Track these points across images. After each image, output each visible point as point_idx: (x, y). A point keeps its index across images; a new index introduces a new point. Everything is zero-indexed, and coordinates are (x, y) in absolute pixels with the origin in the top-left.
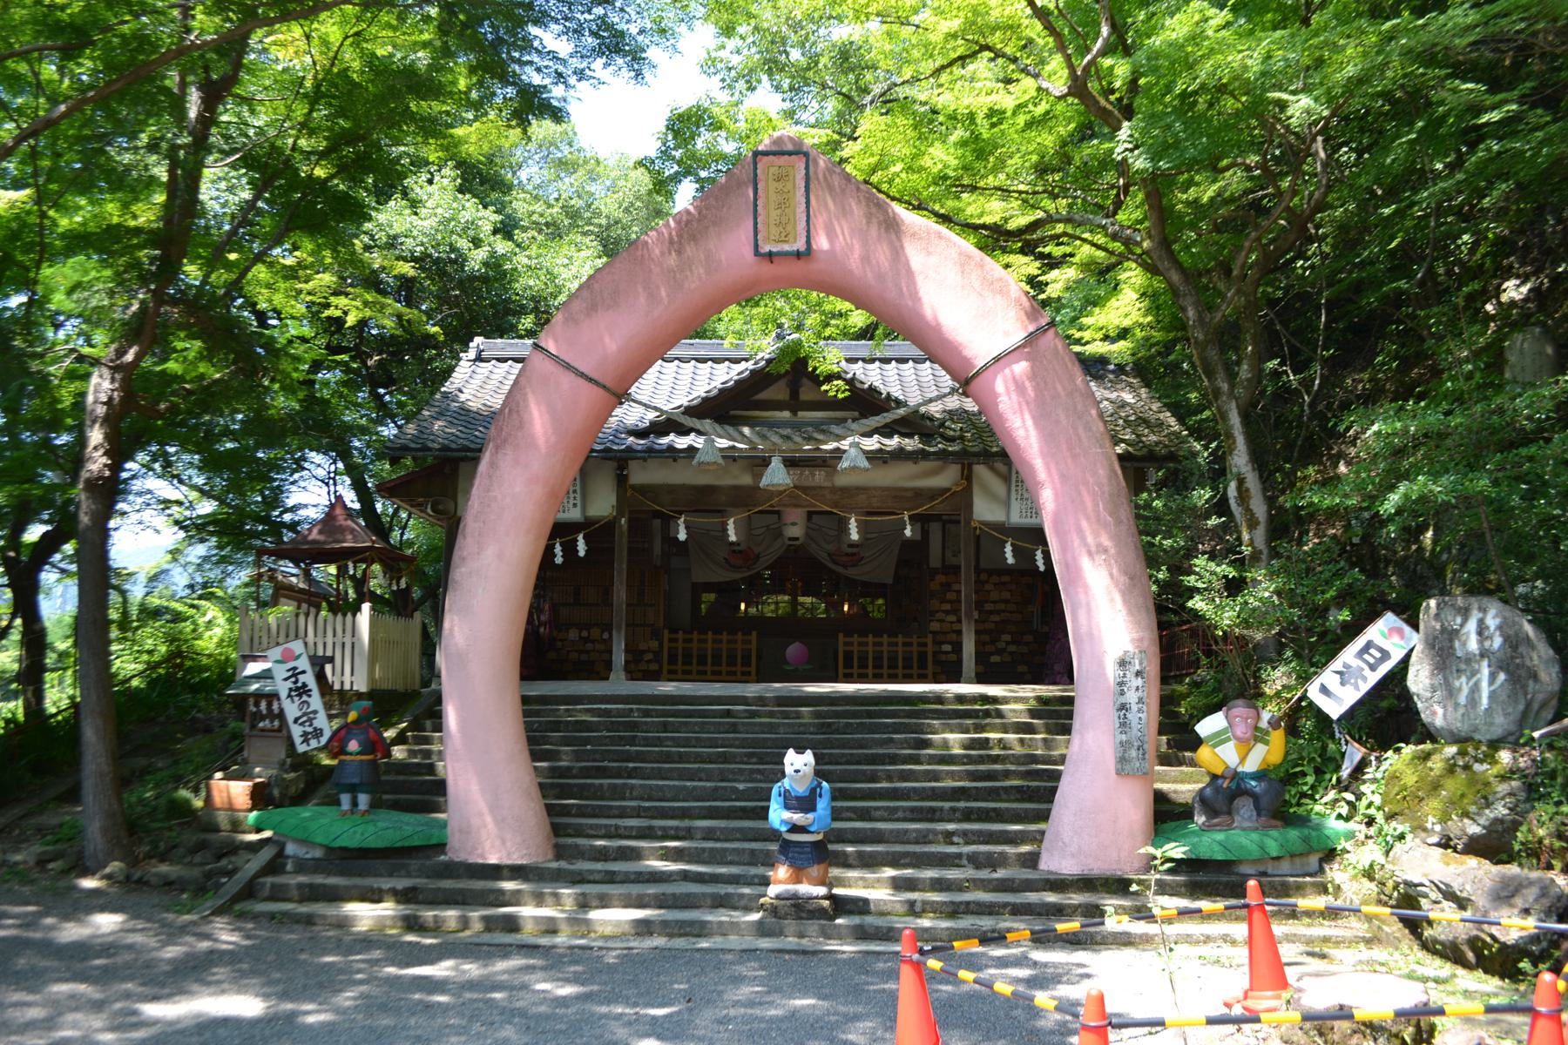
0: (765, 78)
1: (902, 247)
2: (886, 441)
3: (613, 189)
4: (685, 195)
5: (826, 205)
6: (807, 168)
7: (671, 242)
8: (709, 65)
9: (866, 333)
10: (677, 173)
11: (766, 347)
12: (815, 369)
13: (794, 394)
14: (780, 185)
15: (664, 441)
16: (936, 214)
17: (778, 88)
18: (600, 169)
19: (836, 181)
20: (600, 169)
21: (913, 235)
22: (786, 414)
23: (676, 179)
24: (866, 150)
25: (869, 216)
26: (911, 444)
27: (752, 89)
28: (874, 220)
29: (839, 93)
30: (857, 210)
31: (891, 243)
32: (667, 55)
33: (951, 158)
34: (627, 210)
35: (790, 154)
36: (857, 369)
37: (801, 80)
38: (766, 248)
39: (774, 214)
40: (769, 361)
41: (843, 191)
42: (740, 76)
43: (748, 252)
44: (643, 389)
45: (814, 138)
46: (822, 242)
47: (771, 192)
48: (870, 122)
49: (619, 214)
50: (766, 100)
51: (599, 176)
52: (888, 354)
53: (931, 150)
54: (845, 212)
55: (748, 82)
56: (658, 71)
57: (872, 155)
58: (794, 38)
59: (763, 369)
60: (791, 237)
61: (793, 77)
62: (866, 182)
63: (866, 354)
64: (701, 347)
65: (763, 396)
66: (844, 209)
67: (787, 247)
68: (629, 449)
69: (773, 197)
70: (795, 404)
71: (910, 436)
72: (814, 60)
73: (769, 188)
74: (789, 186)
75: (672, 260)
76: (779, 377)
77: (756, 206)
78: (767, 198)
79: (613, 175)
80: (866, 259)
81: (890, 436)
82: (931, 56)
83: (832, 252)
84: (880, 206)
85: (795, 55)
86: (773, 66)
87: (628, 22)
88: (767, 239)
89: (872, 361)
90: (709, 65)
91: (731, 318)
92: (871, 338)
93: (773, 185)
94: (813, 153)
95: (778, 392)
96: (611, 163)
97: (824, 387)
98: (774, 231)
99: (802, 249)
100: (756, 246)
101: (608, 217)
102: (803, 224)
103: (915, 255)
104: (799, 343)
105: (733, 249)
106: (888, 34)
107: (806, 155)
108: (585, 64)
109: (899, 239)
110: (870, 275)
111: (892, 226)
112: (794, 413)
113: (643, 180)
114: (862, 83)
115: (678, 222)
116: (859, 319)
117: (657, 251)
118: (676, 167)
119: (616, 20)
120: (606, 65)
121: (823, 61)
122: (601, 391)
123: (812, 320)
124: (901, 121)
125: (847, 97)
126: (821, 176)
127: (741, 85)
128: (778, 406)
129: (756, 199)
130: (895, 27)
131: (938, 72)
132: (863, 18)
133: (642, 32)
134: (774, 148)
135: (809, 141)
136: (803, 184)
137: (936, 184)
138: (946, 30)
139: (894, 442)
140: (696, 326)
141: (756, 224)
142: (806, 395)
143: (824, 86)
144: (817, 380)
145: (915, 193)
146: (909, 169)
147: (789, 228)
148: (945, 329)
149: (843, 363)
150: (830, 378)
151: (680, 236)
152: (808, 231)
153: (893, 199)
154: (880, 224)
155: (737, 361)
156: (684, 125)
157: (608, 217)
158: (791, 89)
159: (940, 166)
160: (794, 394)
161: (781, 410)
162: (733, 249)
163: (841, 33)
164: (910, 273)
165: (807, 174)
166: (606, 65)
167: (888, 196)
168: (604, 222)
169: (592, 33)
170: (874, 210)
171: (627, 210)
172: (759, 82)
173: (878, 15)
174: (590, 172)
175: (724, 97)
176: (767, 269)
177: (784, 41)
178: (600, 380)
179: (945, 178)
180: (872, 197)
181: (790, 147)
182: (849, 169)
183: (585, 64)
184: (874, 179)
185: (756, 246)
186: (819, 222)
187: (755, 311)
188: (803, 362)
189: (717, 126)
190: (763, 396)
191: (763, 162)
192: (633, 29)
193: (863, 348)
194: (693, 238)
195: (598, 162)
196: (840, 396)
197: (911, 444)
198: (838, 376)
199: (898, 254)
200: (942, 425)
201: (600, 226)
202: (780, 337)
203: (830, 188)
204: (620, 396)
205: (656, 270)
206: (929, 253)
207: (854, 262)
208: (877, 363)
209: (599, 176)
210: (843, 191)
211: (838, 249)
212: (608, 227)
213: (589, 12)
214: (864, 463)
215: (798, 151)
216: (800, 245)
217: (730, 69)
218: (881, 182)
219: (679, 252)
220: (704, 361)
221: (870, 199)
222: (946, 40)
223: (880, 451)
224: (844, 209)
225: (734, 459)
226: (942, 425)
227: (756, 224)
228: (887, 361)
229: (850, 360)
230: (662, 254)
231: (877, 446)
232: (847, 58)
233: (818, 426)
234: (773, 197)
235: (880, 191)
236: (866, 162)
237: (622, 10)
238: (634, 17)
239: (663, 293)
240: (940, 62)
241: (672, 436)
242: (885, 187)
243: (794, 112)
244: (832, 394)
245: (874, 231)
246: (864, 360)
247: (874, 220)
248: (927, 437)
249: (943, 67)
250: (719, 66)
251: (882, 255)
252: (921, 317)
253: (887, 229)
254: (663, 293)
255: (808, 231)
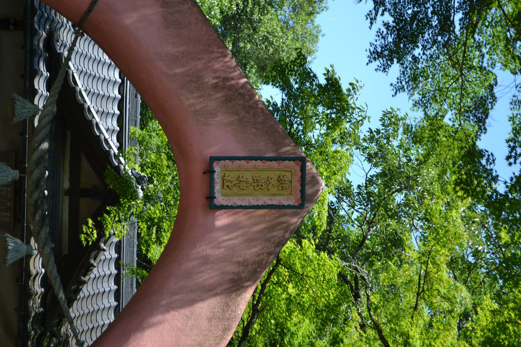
0: (379, 170)
1: (216, 295)
2: (38, 281)
3: (286, 27)
4: (270, 94)
5: (256, 224)
6: (289, 207)
7: (226, 79)
8: (390, 119)
9: (144, 261)
10: (291, 87)
11: (130, 167)
12: (109, 213)
13: (86, 193)
14: (274, 182)
15: (42, 67)
16: (250, 323)
17: (370, 181)
18: (303, 16)
19: (278, 233)
20: (303, 16)
21: (227, 305)
22: (66, 185)
23: (286, 87)
24: (308, 260)
25: (244, 264)
26: (35, 305)
27: (370, 158)
28: (241, 269)
29: (365, 238)
30: (251, 253)
31: (220, 284)
32: (394, 81)
33: (300, 339)
34: (265, 38)
35: (303, 191)
36: (109, 253)
37: (374, 200)
38: (217, 168)
39: (248, 176)
40: (117, 169)
41: (268, 240)
42: (381, 147)
43: (214, 151)
44: (86, 46)
45: (319, 214)
46: (222, 220)
47: (270, 174)
48: (332, 265)
49: (262, 31)
50: (358, 171)
51: (297, 15)
52: (124, 281)
53: (307, 321)
54: (250, 241)
55: (376, 154)
56: (380, 73)
57: (303, 267)
58: (412, 196)
59: (111, 163)
60: (227, 191)
61: (379, 195)
62: (279, 261)
63: (124, 261)
64: (134, 103)
65: (85, 164)
66: (252, 240)
67: (218, 187)
68: (34, 33)
69: (264, 175)
70: (76, 193)
71: (43, 304)
72: (395, 215)
73: (271, 171)
74: (274, 190)
75: (210, 80)
76: (102, 178)
77: (256, 159)
78: (263, 170)
79: (299, 28)
80: (206, 260)
81: (42, 285)
82: (390, 321)
83: (213, 229)
84: (253, 276)
85: (399, 198)
86: (390, 177)
87: (424, 48)
88: (225, 169)
89: (118, 267)
90: (390, 119)
91: (157, 136)
92: (139, 265)
93: (274, 175)
94: (303, 212)
95: (88, 177)
96: (309, 26)
97: (90, 222)
98: (232, 176)
99: (216, 202)
100: (219, 159)
101: (260, 21)
102: (239, 203)
103: (205, 308)
104: (135, 197)
105: (217, 137)
106: (410, 281)
107: (301, 206)
108: (389, 6)
109: (222, 293)
110: (191, 264)
111: (236, 285)
112: (68, 192)
113: (287, 55)
114: (373, 258)
115: (244, 86)
116: (155, 252)
117: (217, 66)
118: (296, 86)
119: (426, 36)
120: (386, 25)
121: (393, 223)
122: (85, 7)
123: (155, 211)
124: (333, 294)
125: (361, 244)
126: (282, 219)
127: (374, 148)
128: (75, 178)
129: (262, 159)
130: (415, 288)
131: (376, 327)
132: (424, 259)
133: (415, 59)
134: (308, 178)
135: (315, 209)
136: (275, 203)
137: (277, 325)
138: (411, 333)
139: (37, 288)
140: (153, 105)
141: (240, 159)
142: (85, 203)
143: (370, 223)
144: (98, 216)
145: (269, 306)
146: (289, 300)
147: (235, 190)
148: (139, 335)
149: (115, 240)
150: (100, 227)
151: (231, 87)
152: (232, 207)
153: (263, 286)
154: (238, 274)
155: (120, 139)
156: (333, 94)
157: (260, 21)
158: (369, 194)
159: (293, 329)
160: (86, 193)
161: (70, 180)
162: (217, 137)
163: (413, 242)
164: (192, 302)
165: (283, 207)
166: (386, 25)
167: (266, 281)
168: (256, 17)
169: (415, 14)
170: (250, 268)
171: (265, 38)
172: (376, 165)
173: (427, 273)
174: (302, 7)
175: (363, 132)
176: (198, 168)
177: (410, 188)
178: (96, 7)
179: (282, 334)
180: (262, 267)
181: (309, 191)
182: (290, 245)
183: (389, 6)
184: (282, 270)
185: (219, 159)
186: (241, 217)
187: (164, 156)
188: (116, 202)
189: (333, 124)
190: (85, 164)
191: (295, 166)
192: (417, 52)
193: (130, 259)
194: (228, 100)
195: (310, 14)
196: (83, 237)
197: (35, 305)
198: (101, 235)
199: (208, 291)
200: (54, 335)
201: (252, 14)
202: (140, 180)
203: (272, 228)
204: (82, 27)
205: (200, 65)
206: (210, 320)
207: (204, 249)
208: (115, 272)
209: (297, 15)
210: (268, 240)
211: (215, 234)
212: (251, 21)
213: (433, 13)
214: (11, 258)
215: (306, 199)
216: (220, 199)
217: (388, 139)
218: (279, 275)
219: (215, 86)
220: (121, 107)
221: (260, 265)
222: (402, 334)
223: (29, 274)
224: (252, 240)
225: (23, 134)
226: (54, 335)
227: (240, 159)
228: (118, 280)
229: (118, 248)
230: (215, 71)
231: (34, 272)
232: (395, 243)
233: (54, 217)
234: (264, 175)
235: (270, 274)
236: (297, 262)
237: (435, 42)
238: (428, 53)
239: (178, 71)
240: (386, 330)
241: (46, 74)
242: (274, 278)
243: (348, 196)
244: (84, 229)
245: (231, 268)
246: (118, 260)
247: (241, 269)
248: (42, 320)
249: (380, 331)
250: (391, 129)
251: (209, 276)
252: (151, 313)
253: (232, 281)
254: (178, 71)
255: (232, 207)
